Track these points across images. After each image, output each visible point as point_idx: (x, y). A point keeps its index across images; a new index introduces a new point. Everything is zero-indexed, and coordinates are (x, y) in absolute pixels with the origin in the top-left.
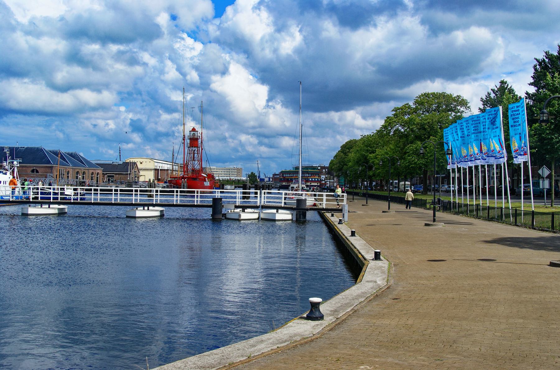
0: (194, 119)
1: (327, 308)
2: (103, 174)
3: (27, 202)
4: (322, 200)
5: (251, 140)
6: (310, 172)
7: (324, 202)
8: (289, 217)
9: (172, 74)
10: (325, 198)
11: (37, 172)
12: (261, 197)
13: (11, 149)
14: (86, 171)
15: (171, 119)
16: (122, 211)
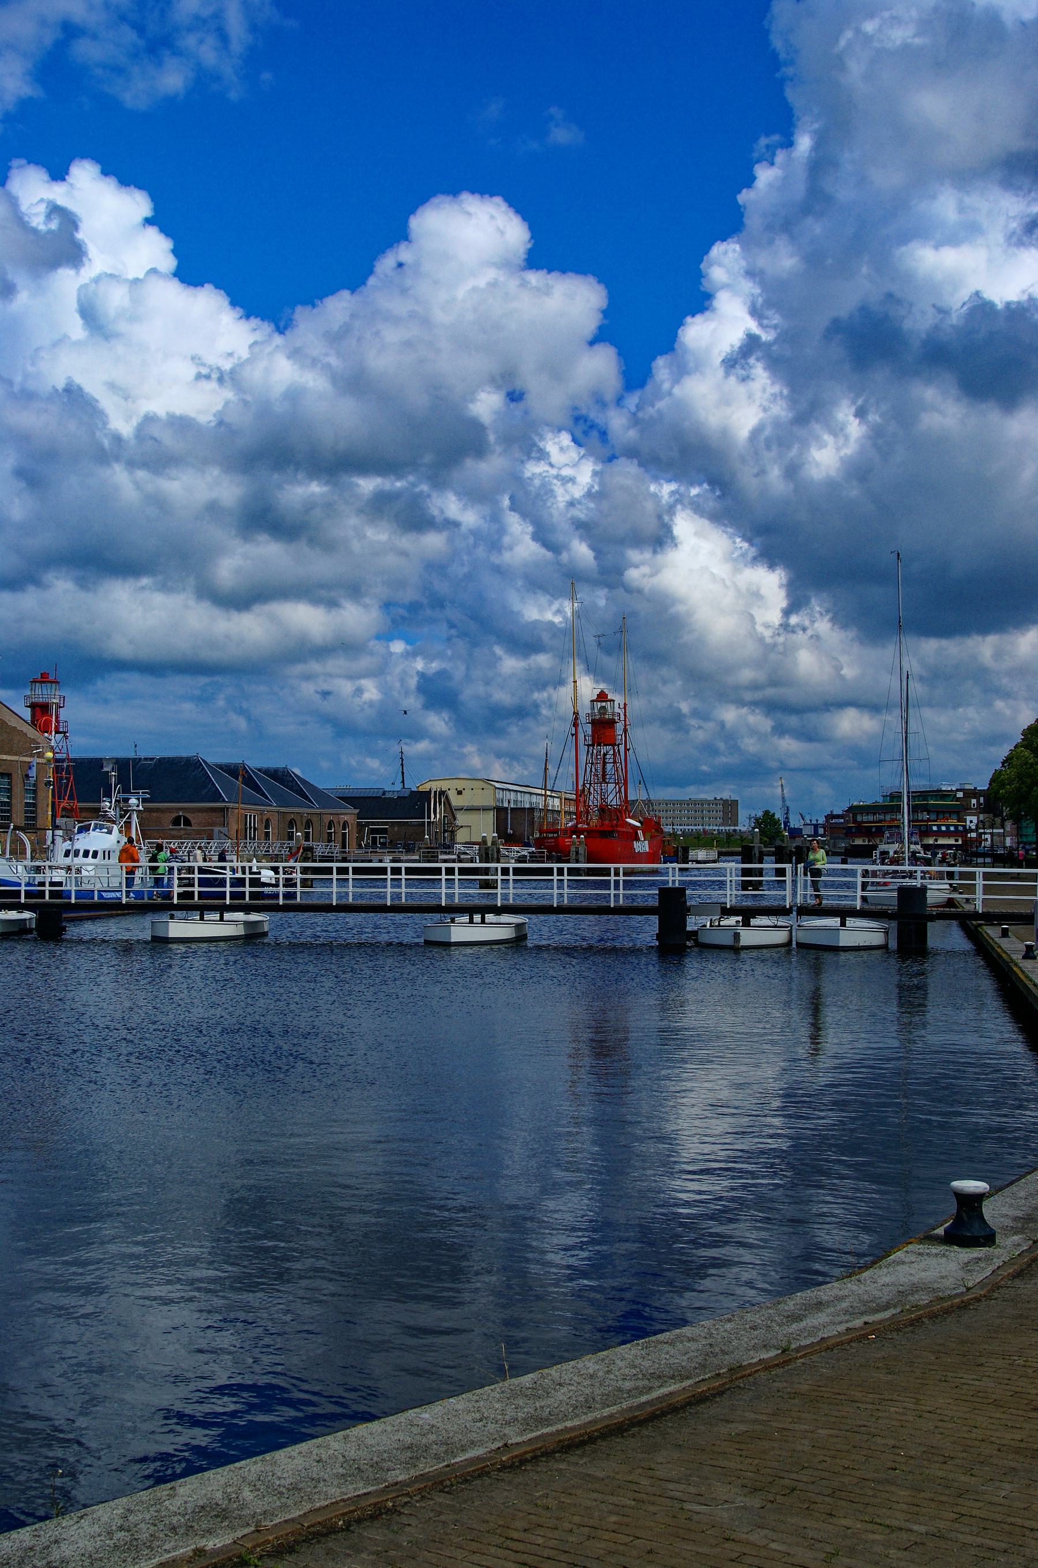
0: (592, 669)
1: (1005, 1210)
2: (360, 827)
3: (161, 905)
4: (971, 889)
5: (752, 719)
6: (933, 806)
7: (979, 896)
8: (876, 939)
9: (522, 546)
10: (980, 882)
11: (188, 822)
12: (794, 882)
13: (122, 765)
14: (315, 819)
15: (528, 670)
16: (410, 929)
